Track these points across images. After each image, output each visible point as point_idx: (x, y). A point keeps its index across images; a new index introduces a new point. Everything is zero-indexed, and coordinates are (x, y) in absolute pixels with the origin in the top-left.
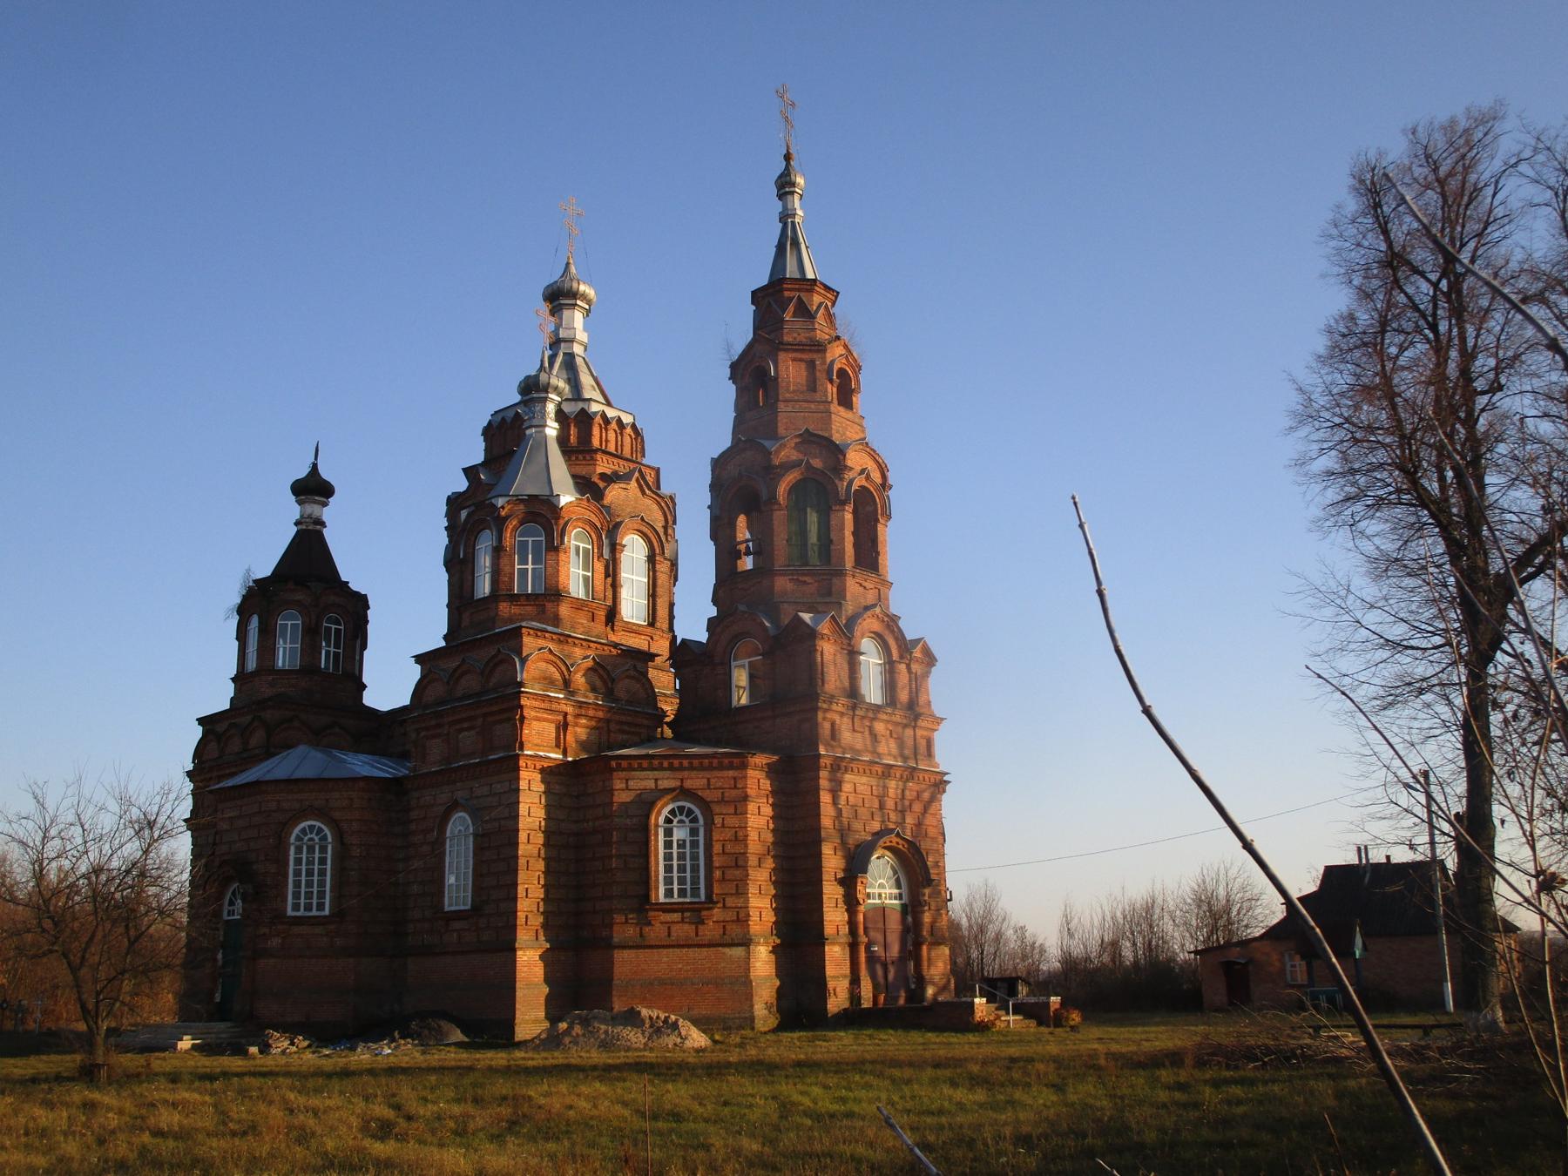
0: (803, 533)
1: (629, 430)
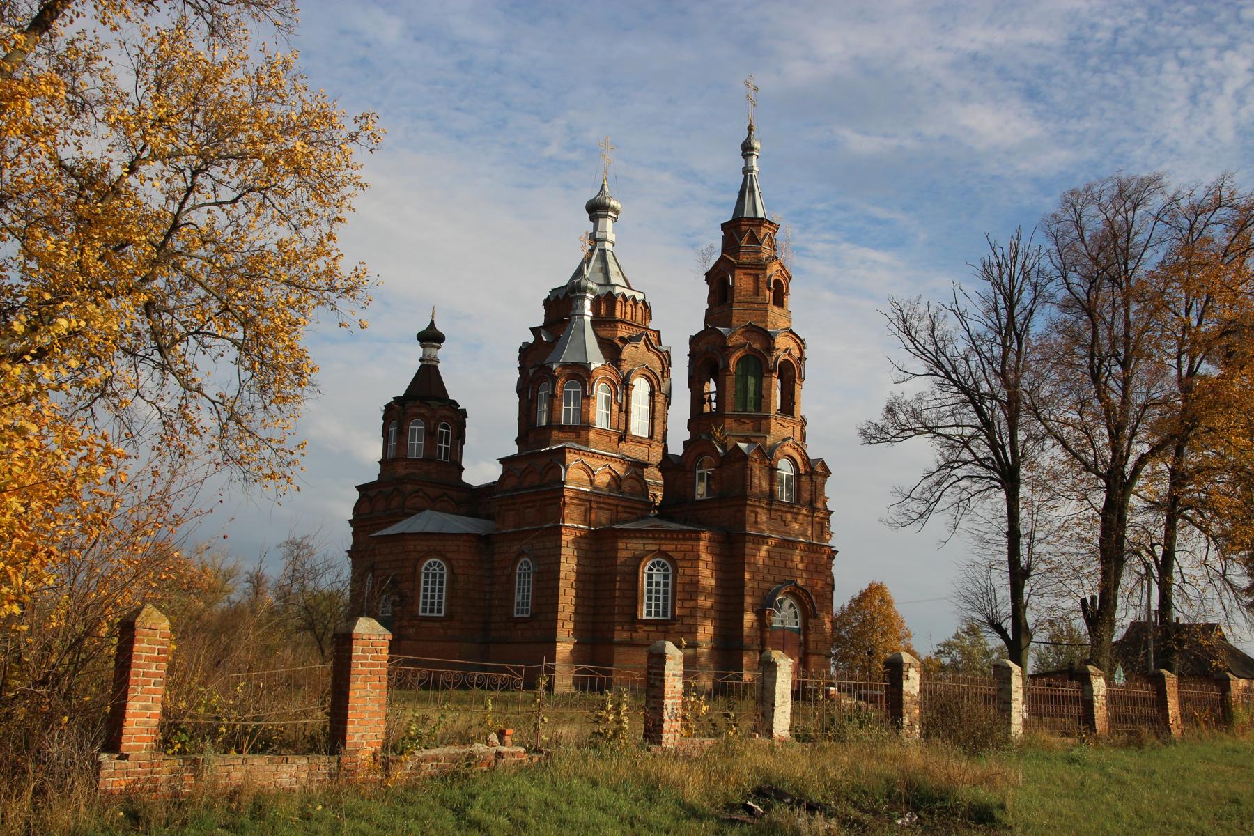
0: (745, 390)
1: (640, 305)
